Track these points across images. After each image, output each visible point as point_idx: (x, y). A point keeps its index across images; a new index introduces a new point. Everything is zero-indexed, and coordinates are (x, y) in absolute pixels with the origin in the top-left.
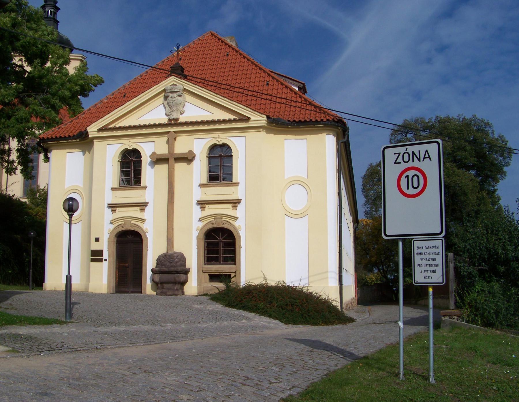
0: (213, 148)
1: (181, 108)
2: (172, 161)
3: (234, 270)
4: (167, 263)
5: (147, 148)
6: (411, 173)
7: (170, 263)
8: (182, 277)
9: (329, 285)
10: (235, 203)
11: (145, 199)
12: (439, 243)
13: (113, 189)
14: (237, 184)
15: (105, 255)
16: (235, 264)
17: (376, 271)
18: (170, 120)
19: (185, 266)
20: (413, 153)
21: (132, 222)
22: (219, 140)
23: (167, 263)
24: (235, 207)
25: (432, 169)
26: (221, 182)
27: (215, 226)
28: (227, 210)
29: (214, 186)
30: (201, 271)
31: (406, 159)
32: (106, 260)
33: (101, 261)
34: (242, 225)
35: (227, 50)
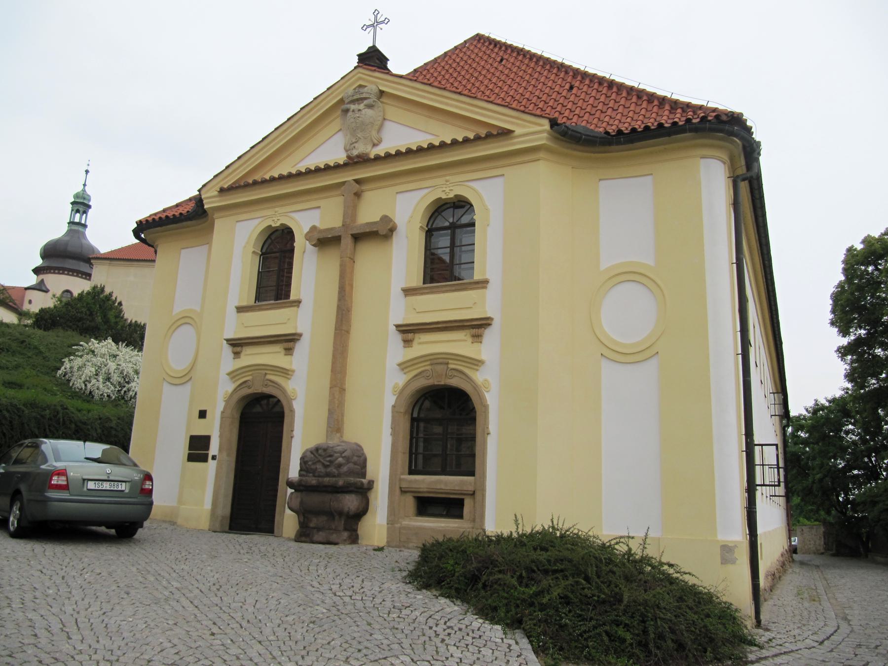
0: (439, 208)
1: (374, 133)
3: (471, 488)
4: (319, 467)
5: (304, 220)
7: (326, 466)
8: (350, 502)
10: (477, 327)
11: (296, 328)
15: (214, 449)
17: (833, 512)
18: (349, 157)
19: (364, 475)
21: (268, 377)
22: (447, 190)
23: (319, 467)
28: (457, 344)
29: (432, 291)
30: (399, 490)
32: (214, 458)
33: (204, 459)
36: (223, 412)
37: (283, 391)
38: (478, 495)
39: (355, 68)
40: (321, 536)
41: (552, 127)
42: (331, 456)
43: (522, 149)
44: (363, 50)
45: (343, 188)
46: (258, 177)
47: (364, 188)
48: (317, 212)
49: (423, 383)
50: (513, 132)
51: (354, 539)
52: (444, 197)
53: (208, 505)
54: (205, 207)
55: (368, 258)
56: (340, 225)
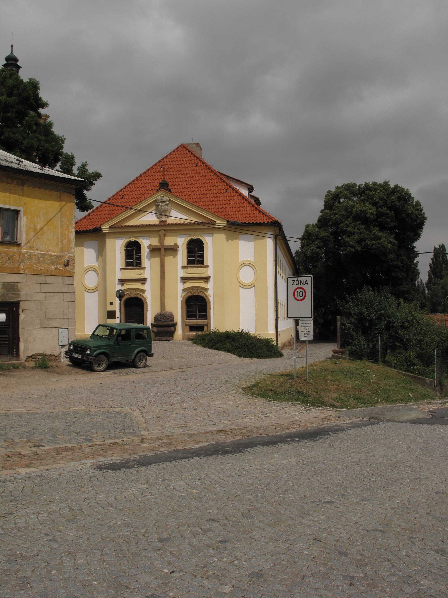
2: (163, 251)
4: (162, 319)
5: (145, 243)
6: (299, 290)
8: (172, 328)
9: (269, 332)
12: (310, 322)
13: (122, 269)
14: (207, 266)
15: (118, 314)
16: (207, 319)
18: (160, 221)
19: (173, 321)
20: (301, 281)
24: (143, 284)
25: (308, 288)
26: (196, 264)
28: (201, 284)
29: (191, 267)
30: (185, 325)
31: (297, 284)
32: (118, 318)
34: (211, 292)
35: (197, 161)
37: (143, 297)
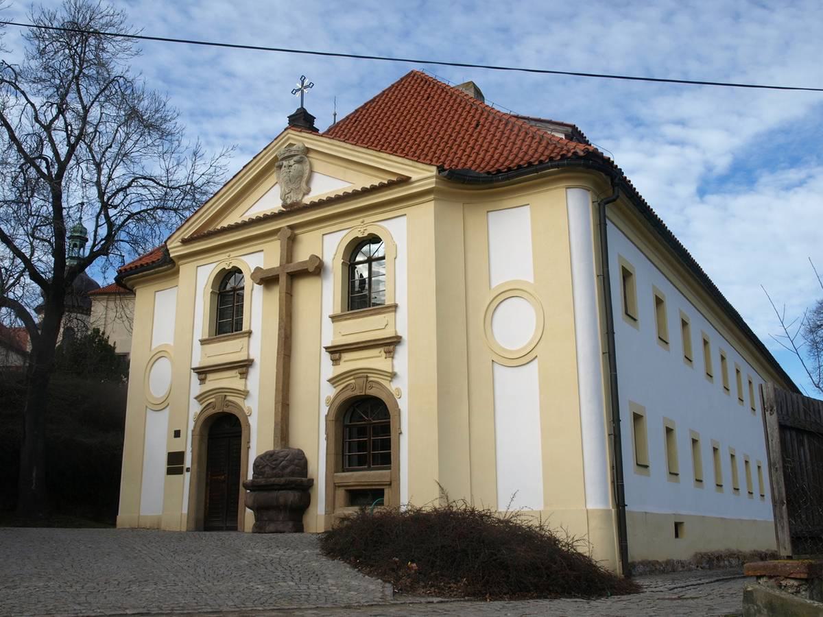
0: (356, 245)
10: (391, 344)
15: (188, 462)
21: (228, 398)
24: (390, 354)
27: (357, 393)
29: (353, 317)
30: (333, 486)
32: (188, 470)
36: (327, 416)
37: (241, 409)
38: (332, 485)
39: (285, 130)
40: (272, 527)
41: (439, 172)
42: (276, 460)
43: (181, 255)
44: (293, 112)
45: (279, 234)
46: (211, 229)
47: (297, 232)
48: (261, 254)
49: (349, 394)
50: (410, 178)
51: (299, 528)
52: (360, 235)
53: (185, 511)
54: (171, 256)
55: (305, 289)
56: (278, 265)
